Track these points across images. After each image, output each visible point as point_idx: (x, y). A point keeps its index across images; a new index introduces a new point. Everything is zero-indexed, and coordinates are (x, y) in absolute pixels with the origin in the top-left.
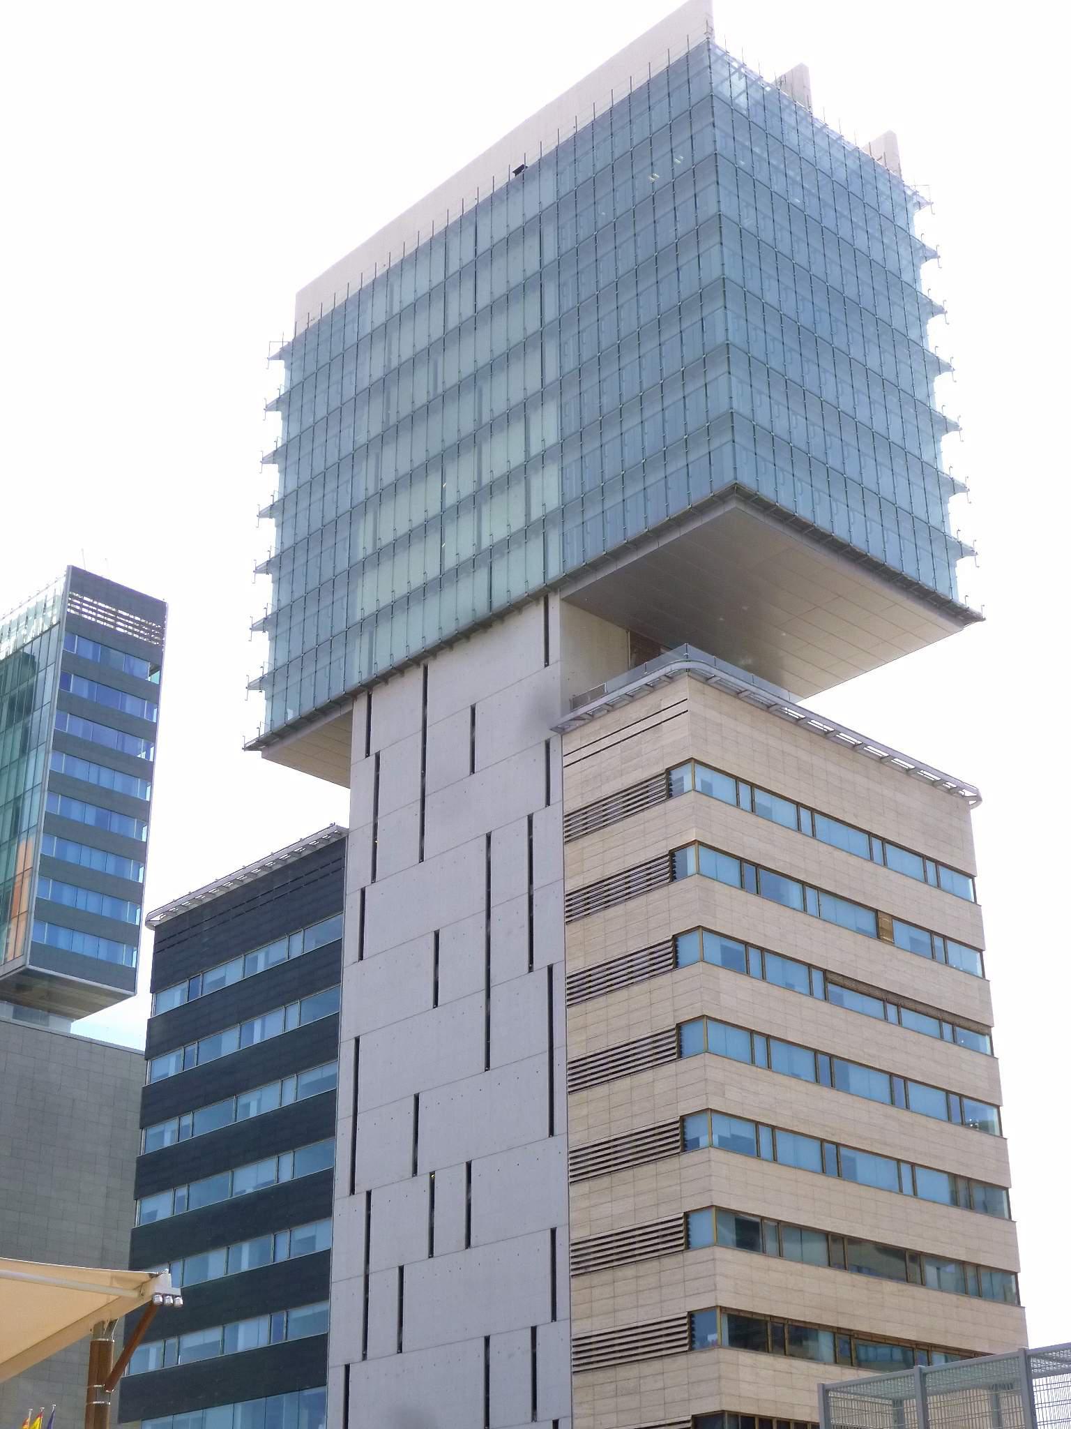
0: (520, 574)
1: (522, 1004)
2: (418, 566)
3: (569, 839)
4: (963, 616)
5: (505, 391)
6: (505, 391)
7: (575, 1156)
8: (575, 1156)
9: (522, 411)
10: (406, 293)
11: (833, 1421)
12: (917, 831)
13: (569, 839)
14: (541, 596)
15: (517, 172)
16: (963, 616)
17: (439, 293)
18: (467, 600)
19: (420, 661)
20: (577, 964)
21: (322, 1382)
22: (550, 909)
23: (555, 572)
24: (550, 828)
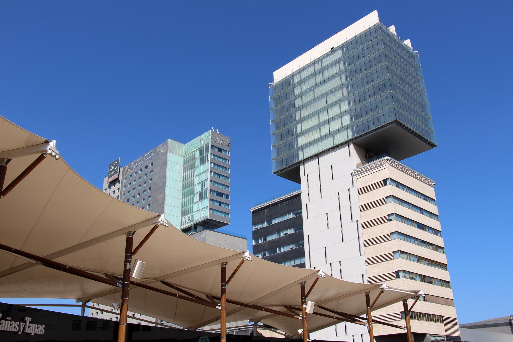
0: (342, 137)
1: (350, 229)
2: (314, 135)
3: (359, 194)
4: (433, 146)
5: (332, 99)
6: (332, 99)
7: (367, 260)
8: (367, 260)
9: (339, 102)
10: (304, 75)
11: (301, 167)
13: (359, 194)
14: (347, 143)
15: (332, 49)
16: (433, 146)
17: (314, 75)
18: (328, 144)
19: (317, 156)
20: (364, 221)
21: (303, 240)
22: (356, 210)
23: (350, 137)
24: (354, 192)
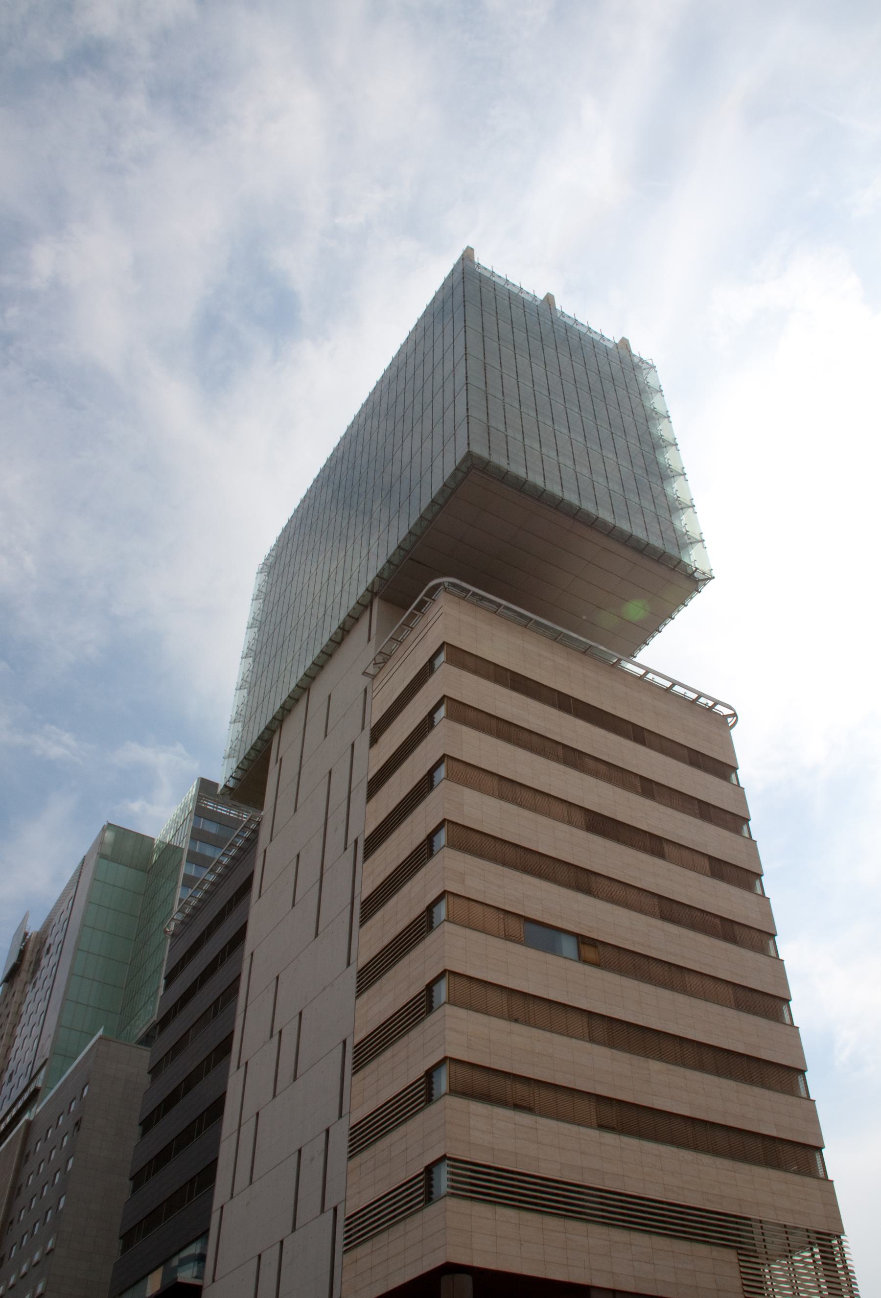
12: (693, 750)
